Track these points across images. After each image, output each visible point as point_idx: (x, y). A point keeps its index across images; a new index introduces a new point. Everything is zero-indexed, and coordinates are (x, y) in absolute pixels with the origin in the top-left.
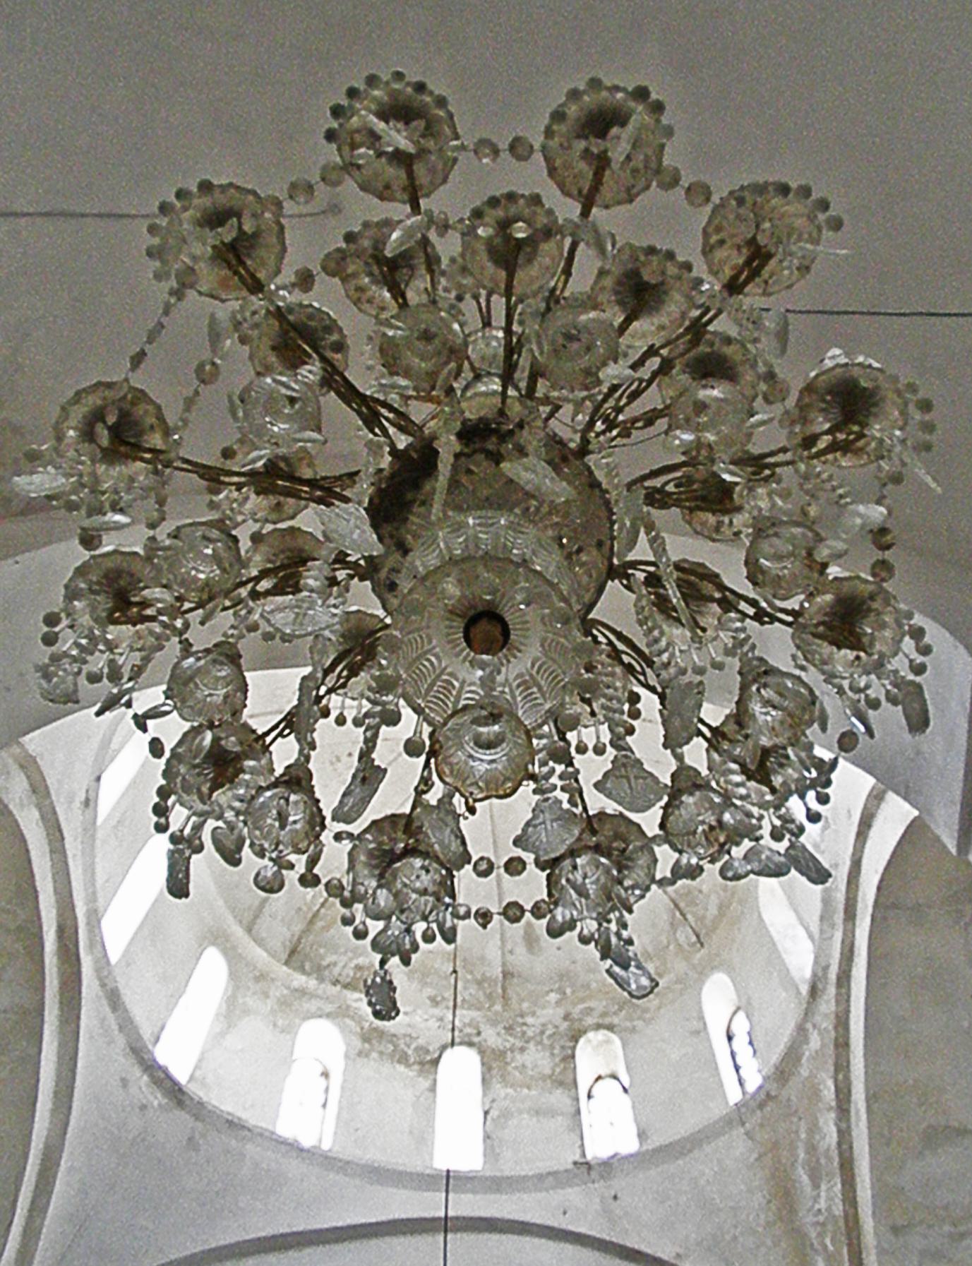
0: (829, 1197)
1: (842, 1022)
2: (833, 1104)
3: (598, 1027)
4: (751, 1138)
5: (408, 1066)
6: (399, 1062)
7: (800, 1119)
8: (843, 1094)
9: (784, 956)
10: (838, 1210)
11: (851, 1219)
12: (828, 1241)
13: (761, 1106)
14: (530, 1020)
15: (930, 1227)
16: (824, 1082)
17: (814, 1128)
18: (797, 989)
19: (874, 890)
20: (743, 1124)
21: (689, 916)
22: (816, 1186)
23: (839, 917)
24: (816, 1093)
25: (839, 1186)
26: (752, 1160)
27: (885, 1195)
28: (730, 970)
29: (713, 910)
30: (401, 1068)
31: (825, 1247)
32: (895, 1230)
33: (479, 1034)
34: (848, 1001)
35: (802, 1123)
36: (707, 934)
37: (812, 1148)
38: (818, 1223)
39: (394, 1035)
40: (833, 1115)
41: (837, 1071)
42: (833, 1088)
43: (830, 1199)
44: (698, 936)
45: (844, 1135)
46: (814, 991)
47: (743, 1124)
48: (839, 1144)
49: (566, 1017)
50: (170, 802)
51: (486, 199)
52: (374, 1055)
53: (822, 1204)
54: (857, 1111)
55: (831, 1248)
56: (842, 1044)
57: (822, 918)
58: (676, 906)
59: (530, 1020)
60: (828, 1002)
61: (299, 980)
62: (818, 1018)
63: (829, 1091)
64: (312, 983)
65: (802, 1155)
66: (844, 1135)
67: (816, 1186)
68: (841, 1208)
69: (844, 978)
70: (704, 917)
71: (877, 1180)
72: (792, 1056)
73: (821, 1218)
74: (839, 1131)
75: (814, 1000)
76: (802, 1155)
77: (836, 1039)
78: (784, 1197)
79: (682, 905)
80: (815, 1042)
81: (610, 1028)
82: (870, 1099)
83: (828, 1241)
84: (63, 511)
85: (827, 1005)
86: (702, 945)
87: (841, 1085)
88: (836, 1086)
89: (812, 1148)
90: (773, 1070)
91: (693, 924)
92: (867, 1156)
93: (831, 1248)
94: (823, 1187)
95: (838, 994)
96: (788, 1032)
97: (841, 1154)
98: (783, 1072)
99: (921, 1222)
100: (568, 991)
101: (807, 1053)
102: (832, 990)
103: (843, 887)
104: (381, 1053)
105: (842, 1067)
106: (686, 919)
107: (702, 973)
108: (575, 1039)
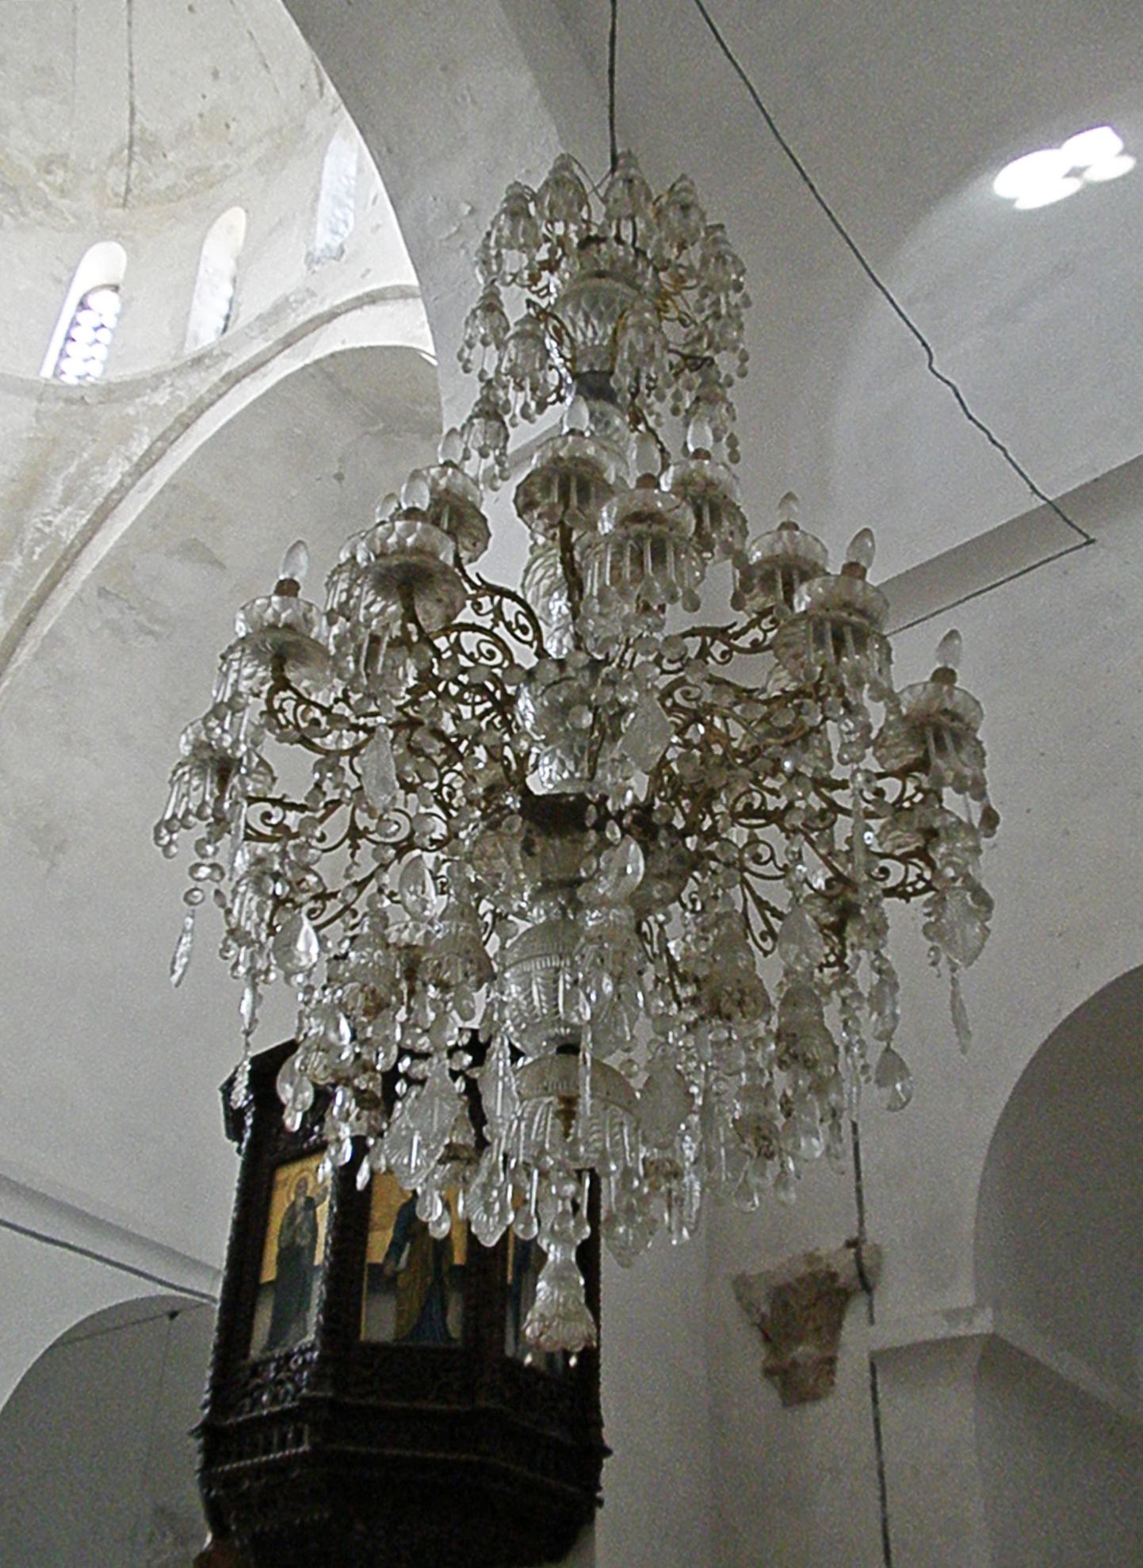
0: (69, 522)
1: (200, 408)
2: (135, 459)
4: (38, 420)
7: (94, 441)
8: (149, 460)
9: (196, 302)
10: (69, 536)
11: (74, 550)
13: (69, 401)
15: (131, 608)
16: (141, 433)
17: (101, 460)
18: (183, 343)
19: (328, 351)
20: (40, 400)
21: (134, 165)
22: (65, 502)
23: (278, 333)
24: (125, 439)
25: (84, 521)
26: (25, 435)
27: (117, 563)
28: (133, 253)
29: (161, 184)
32: (103, 592)
34: (220, 396)
35: (94, 447)
36: (139, 198)
37: (84, 473)
40: (127, 467)
41: (161, 438)
42: (145, 447)
43: (69, 524)
44: (128, 191)
46: (198, 361)
47: (40, 400)
48: (113, 491)
50: (449, 653)
53: (57, 520)
54: (149, 484)
56: (185, 424)
57: (259, 318)
58: (131, 146)
60: (203, 381)
62: (179, 383)
65: (72, 469)
67: (65, 502)
68: (72, 537)
69: (234, 379)
70: (148, 181)
71: (121, 547)
72: (131, 389)
73: (47, 530)
74: (121, 483)
75: (191, 366)
76: (72, 469)
77: (183, 415)
78: (30, 488)
79: (136, 149)
80: (161, 398)
82: (171, 486)
85: (202, 383)
87: (155, 450)
88: (150, 447)
89: (84, 473)
90: (103, 383)
91: (133, 177)
92: (129, 522)
94: (69, 509)
95: (216, 386)
96: (147, 368)
97: (107, 499)
98: (111, 393)
99: (127, 601)
101: (146, 399)
103: (302, 319)
105: (167, 440)
106: (129, 164)
107: (106, 232)
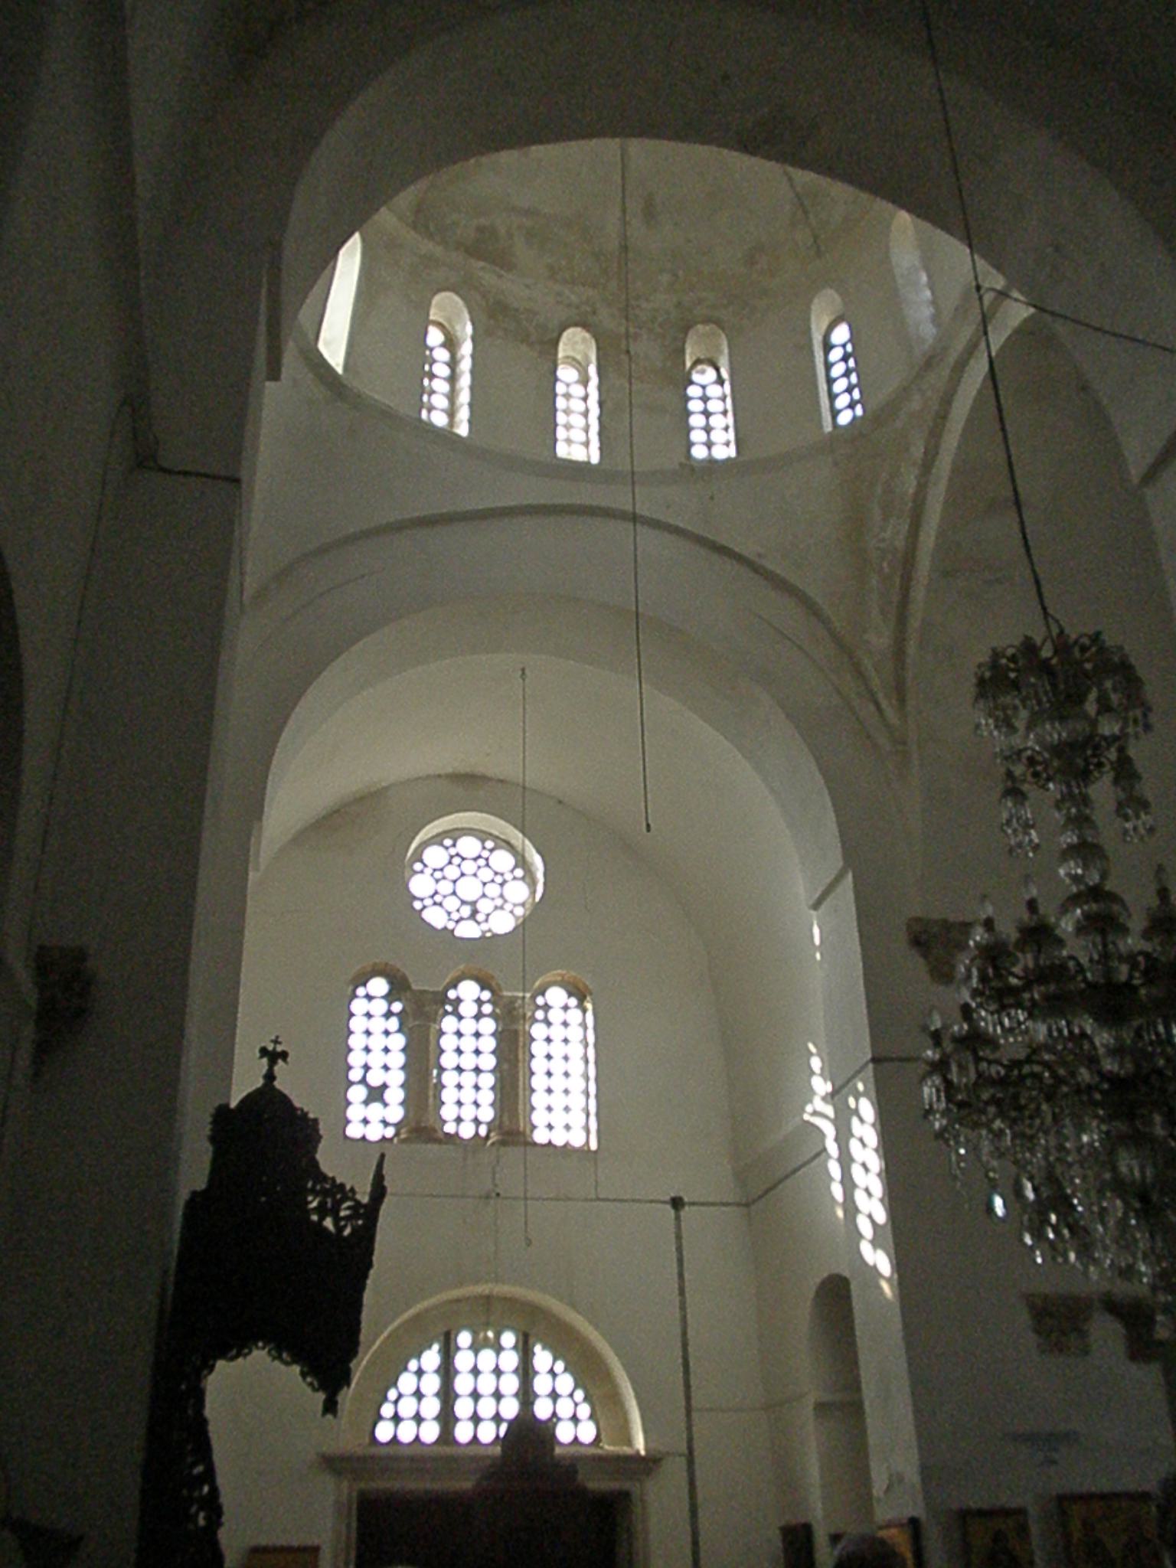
0: (895, 533)
1: (947, 400)
3: (707, 321)
5: (531, 345)
6: (522, 342)
10: (900, 543)
12: (885, 565)
14: (644, 305)
22: (885, 519)
30: (524, 348)
31: (882, 568)
33: (594, 313)
38: (878, 548)
39: (517, 310)
45: (922, 488)
48: (916, 494)
49: (679, 304)
51: (1133, 661)
52: (500, 333)
53: (887, 535)
55: (887, 570)
56: (943, 416)
59: (644, 305)
61: (427, 246)
63: (918, 451)
64: (438, 251)
66: (922, 488)
67: (885, 519)
80: (916, 404)
81: (718, 323)
83: (885, 565)
84: (686, 1199)
86: (819, 254)
93: (887, 570)
100: (681, 273)
102: (946, 373)
104: (505, 330)
105: (935, 435)
108: (686, 329)
